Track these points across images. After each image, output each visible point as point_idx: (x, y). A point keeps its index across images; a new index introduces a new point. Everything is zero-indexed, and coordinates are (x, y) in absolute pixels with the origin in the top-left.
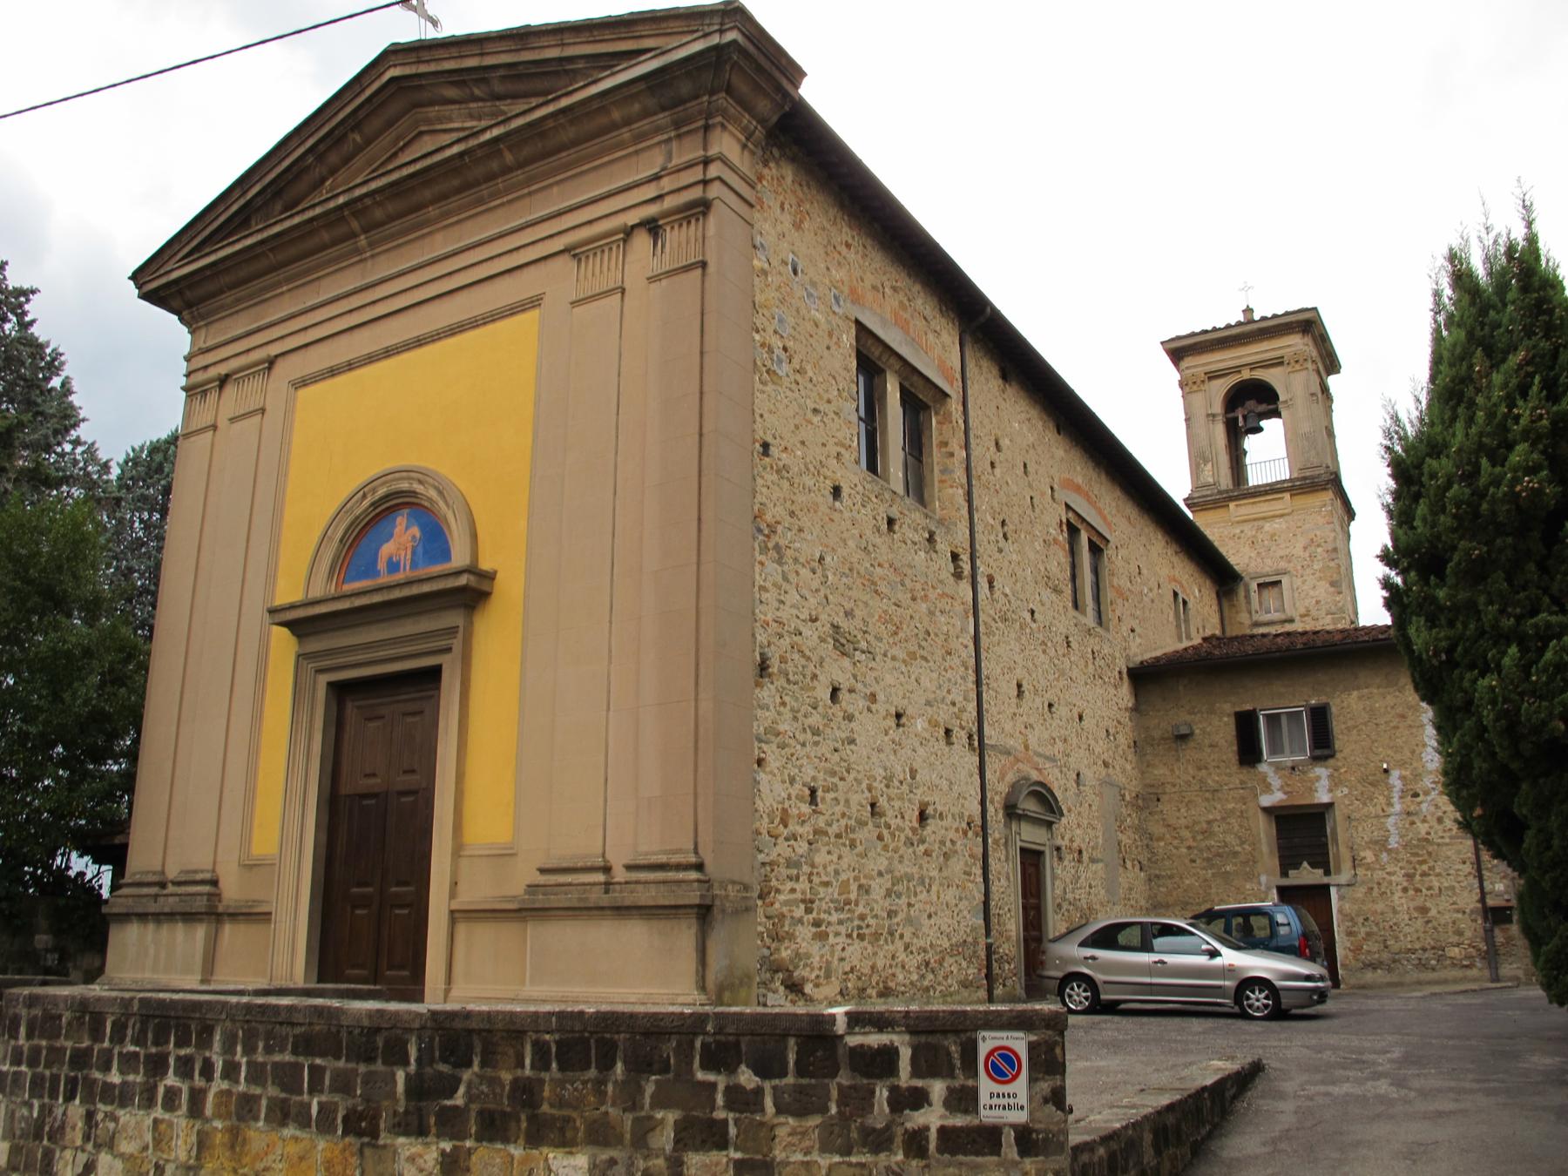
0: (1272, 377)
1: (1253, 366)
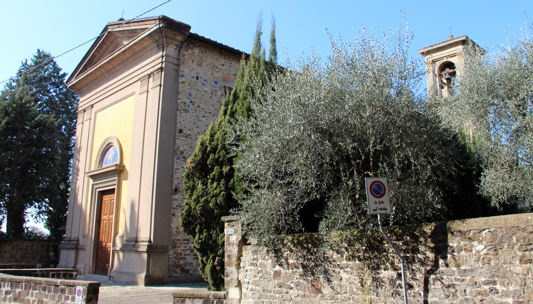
0: (452, 60)
1: (447, 57)
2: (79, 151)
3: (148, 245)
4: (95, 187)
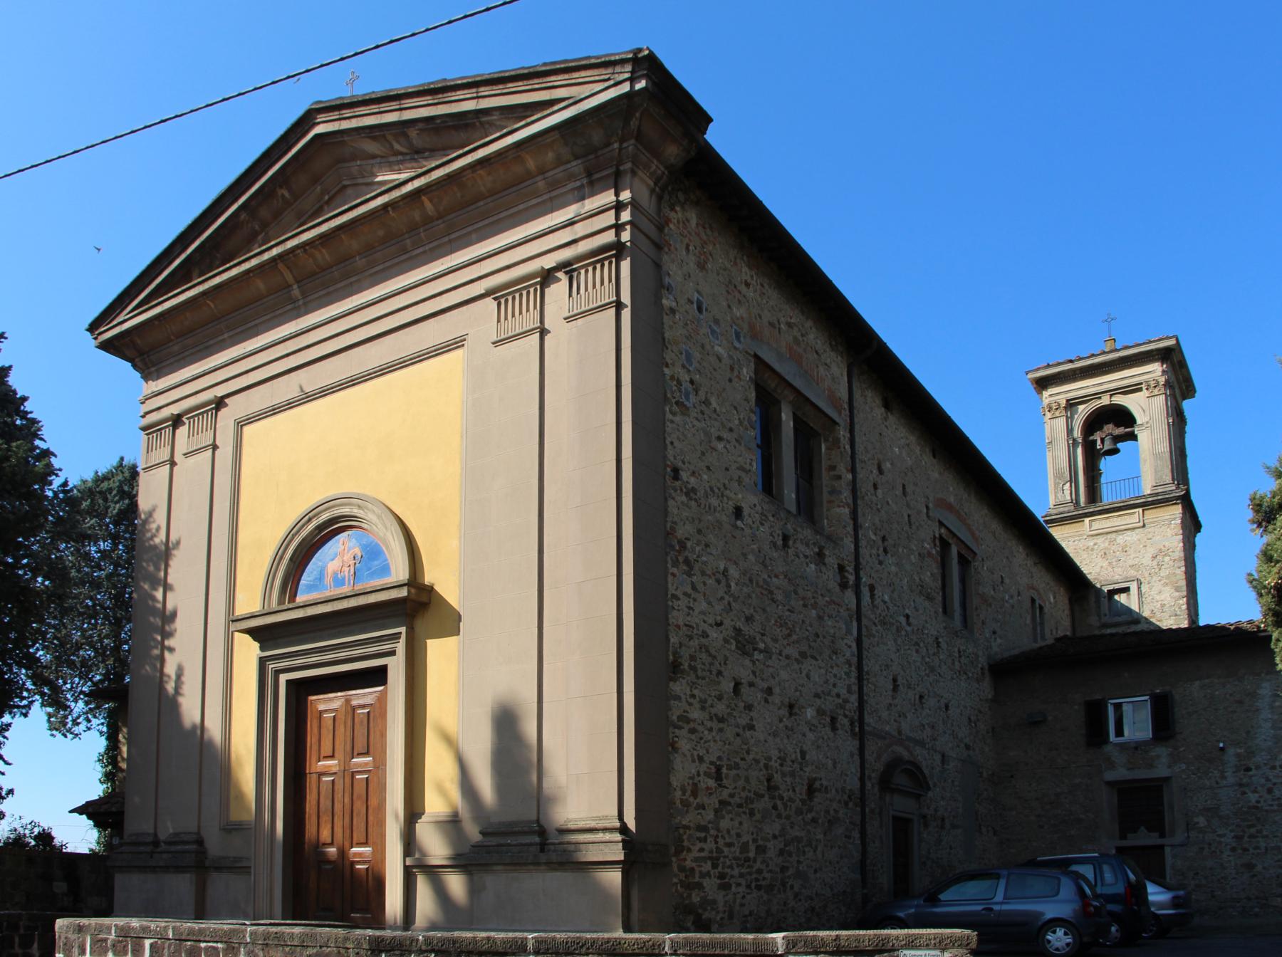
0: (1131, 402)
1: (1113, 392)
2: (165, 554)
3: (623, 841)
4: (272, 666)
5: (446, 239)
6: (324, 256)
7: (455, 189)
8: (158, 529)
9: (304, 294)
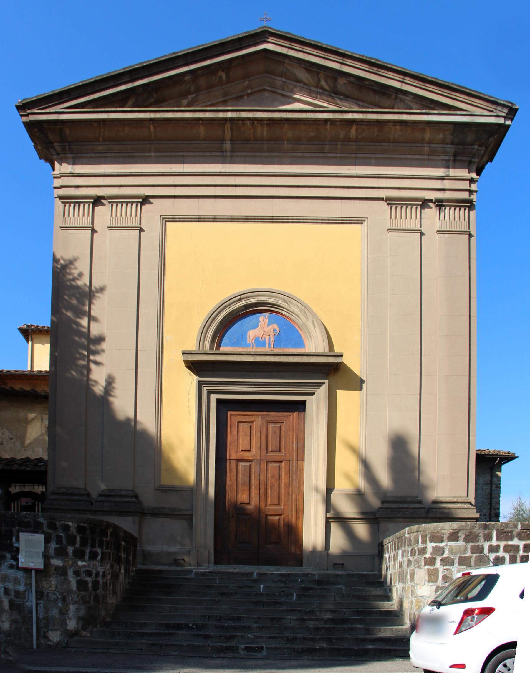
4: (205, 389)
5: (354, 155)
6: (265, 132)
7: (376, 130)
8: (81, 275)
9: (233, 150)
